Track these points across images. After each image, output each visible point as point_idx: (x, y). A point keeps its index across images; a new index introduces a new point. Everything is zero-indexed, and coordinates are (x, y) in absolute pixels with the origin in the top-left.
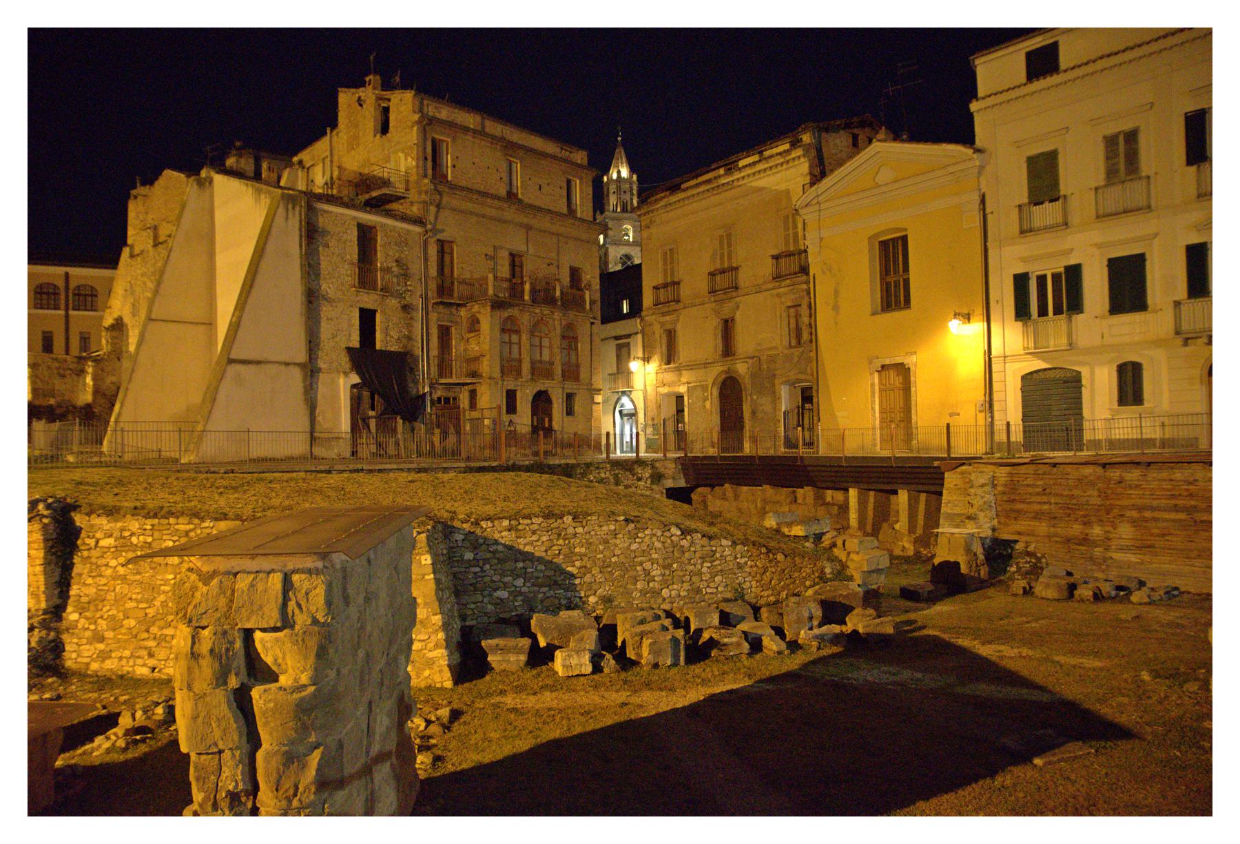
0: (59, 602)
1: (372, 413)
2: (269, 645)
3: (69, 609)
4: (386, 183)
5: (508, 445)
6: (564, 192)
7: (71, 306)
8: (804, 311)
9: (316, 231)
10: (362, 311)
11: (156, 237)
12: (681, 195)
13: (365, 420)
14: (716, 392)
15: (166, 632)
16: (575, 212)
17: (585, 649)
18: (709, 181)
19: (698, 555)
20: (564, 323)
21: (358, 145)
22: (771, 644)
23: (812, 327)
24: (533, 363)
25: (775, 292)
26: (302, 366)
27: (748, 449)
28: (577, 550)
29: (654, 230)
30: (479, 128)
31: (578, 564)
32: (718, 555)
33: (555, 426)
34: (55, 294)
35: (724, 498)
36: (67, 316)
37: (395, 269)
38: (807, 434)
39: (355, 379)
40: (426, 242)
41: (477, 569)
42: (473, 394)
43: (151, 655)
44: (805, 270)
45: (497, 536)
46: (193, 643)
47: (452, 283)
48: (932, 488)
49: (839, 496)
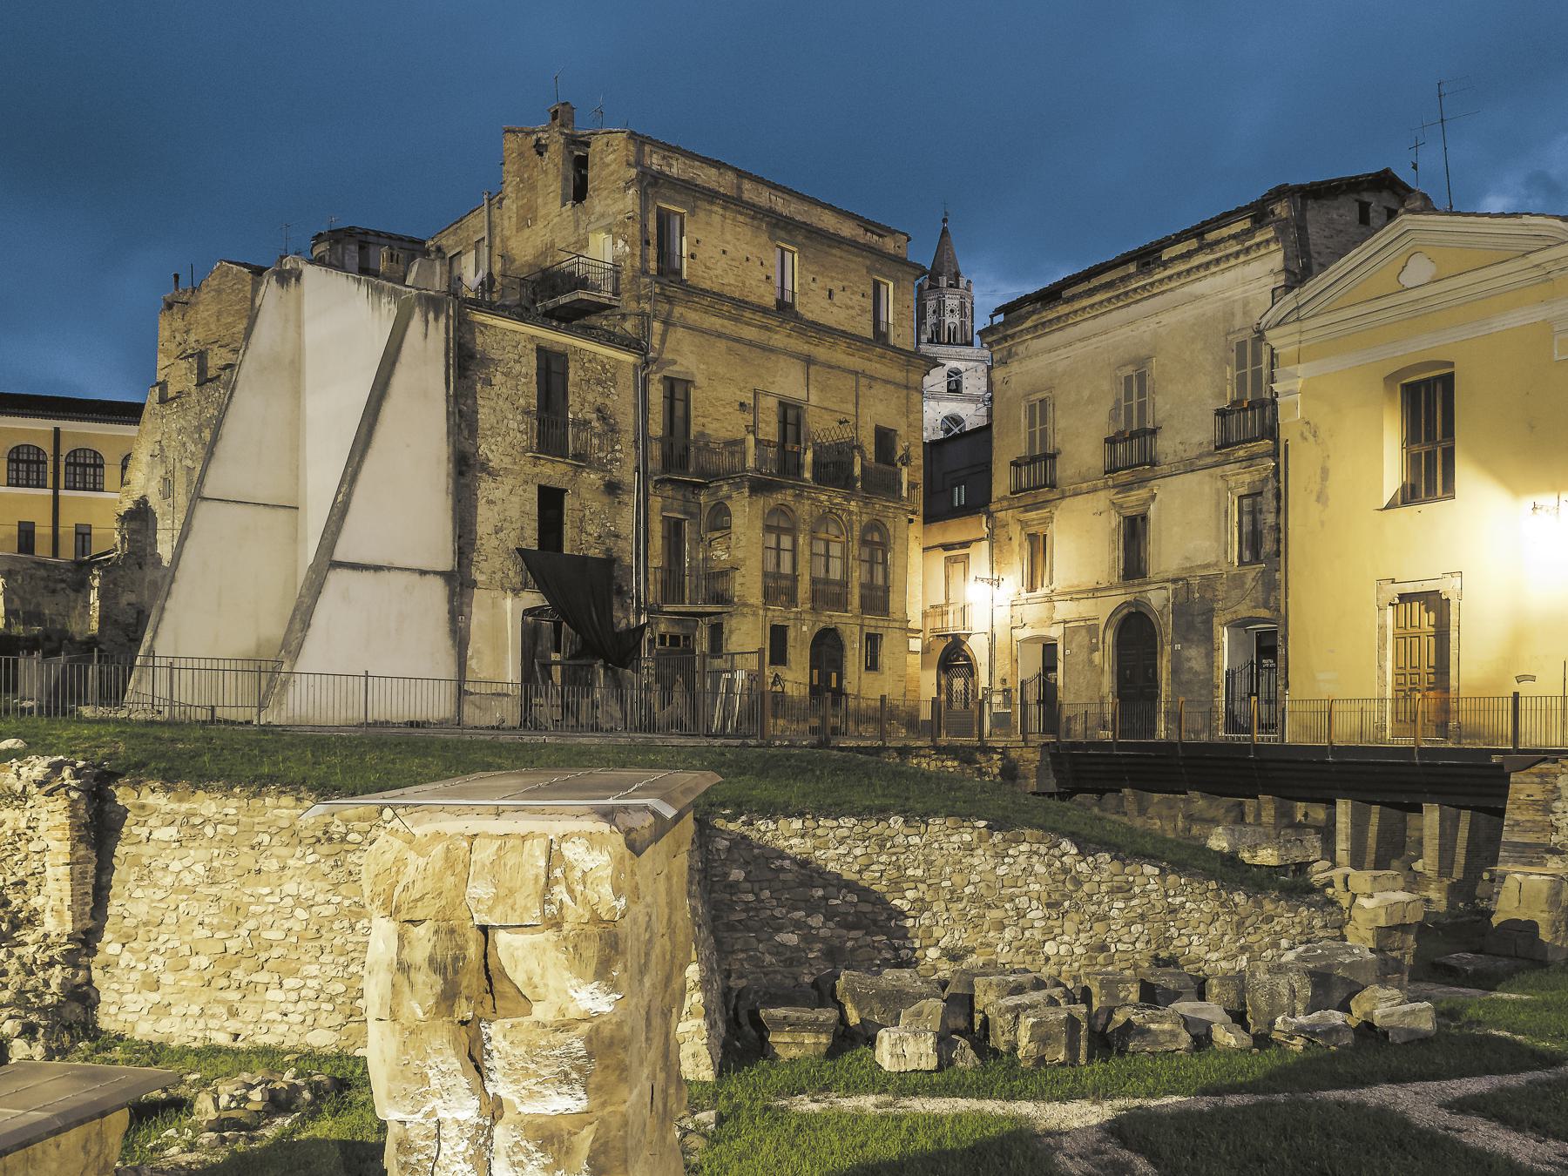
0: (90, 924)
1: (555, 657)
2: (520, 953)
3: (107, 936)
4: (583, 283)
5: (775, 716)
6: (868, 303)
7: (62, 484)
8: (1268, 502)
9: (472, 356)
10: (543, 491)
11: (202, 370)
12: (1063, 309)
13: (547, 667)
14: (1110, 637)
15: (256, 977)
16: (886, 335)
17: (926, 1031)
18: (1110, 285)
19: (1104, 888)
20: (865, 518)
21: (534, 220)
22: (1227, 1037)
23: (1280, 531)
24: (814, 581)
25: (1218, 471)
26: (447, 576)
27: (1162, 731)
28: (910, 872)
29: (1015, 367)
30: (734, 193)
31: (910, 894)
32: (1137, 890)
33: (850, 686)
34: (38, 462)
35: (1120, 810)
36: (56, 498)
37: (595, 424)
38: (1264, 707)
39: (533, 599)
40: (646, 381)
41: (751, 897)
42: (717, 632)
43: (233, 1013)
44: (1271, 432)
45: (782, 843)
46: (401, 947)
47: (687, 449)
48: (1483, 802)
49: (1319, 813)
